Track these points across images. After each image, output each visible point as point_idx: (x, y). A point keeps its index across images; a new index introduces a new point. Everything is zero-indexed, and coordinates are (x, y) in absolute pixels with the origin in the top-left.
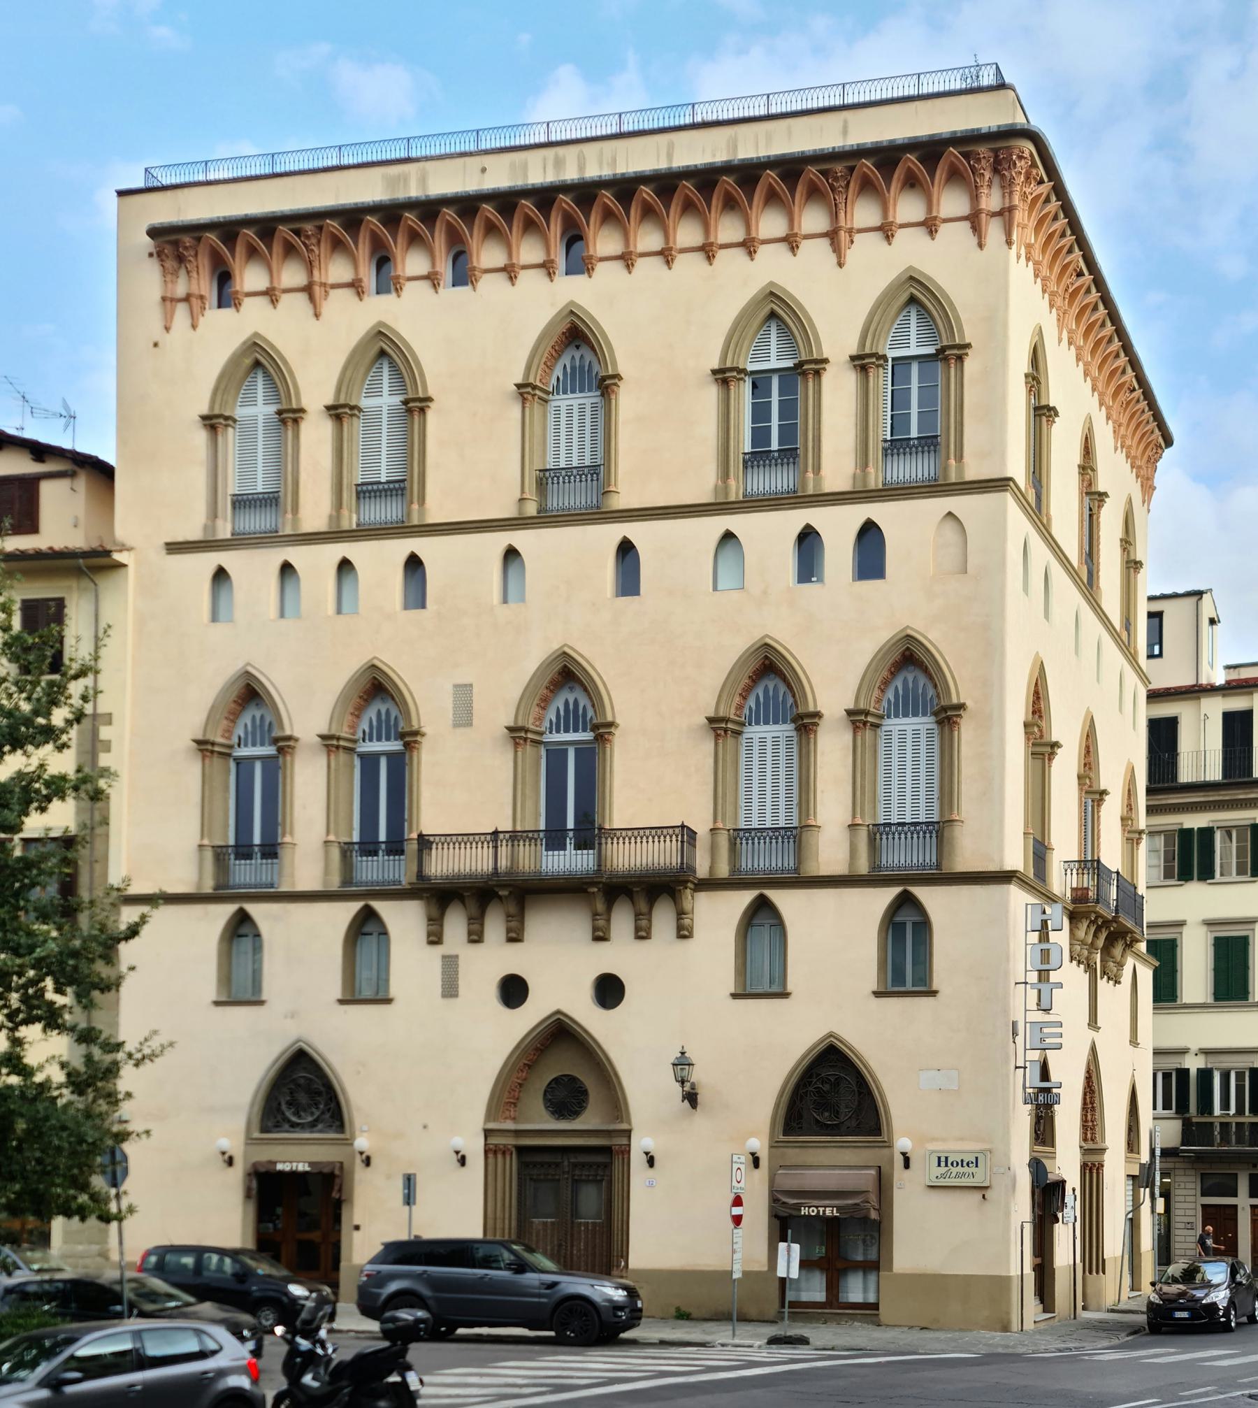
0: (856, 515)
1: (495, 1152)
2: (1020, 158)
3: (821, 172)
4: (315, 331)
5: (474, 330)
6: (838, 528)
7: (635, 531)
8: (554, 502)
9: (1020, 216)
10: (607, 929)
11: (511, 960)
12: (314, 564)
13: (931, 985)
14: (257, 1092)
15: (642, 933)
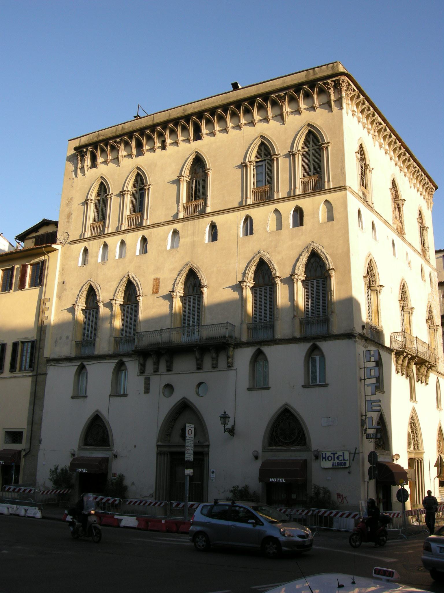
2: (343, 82)
3: (323, 84)
4: (118, 171)
5: (166, 163)
6: (287, 209)
7: (218, 219)
9: (344, 101)
11: (167, 378)
12: (114, 242)
13: (325, 382)
14: (83, 429)
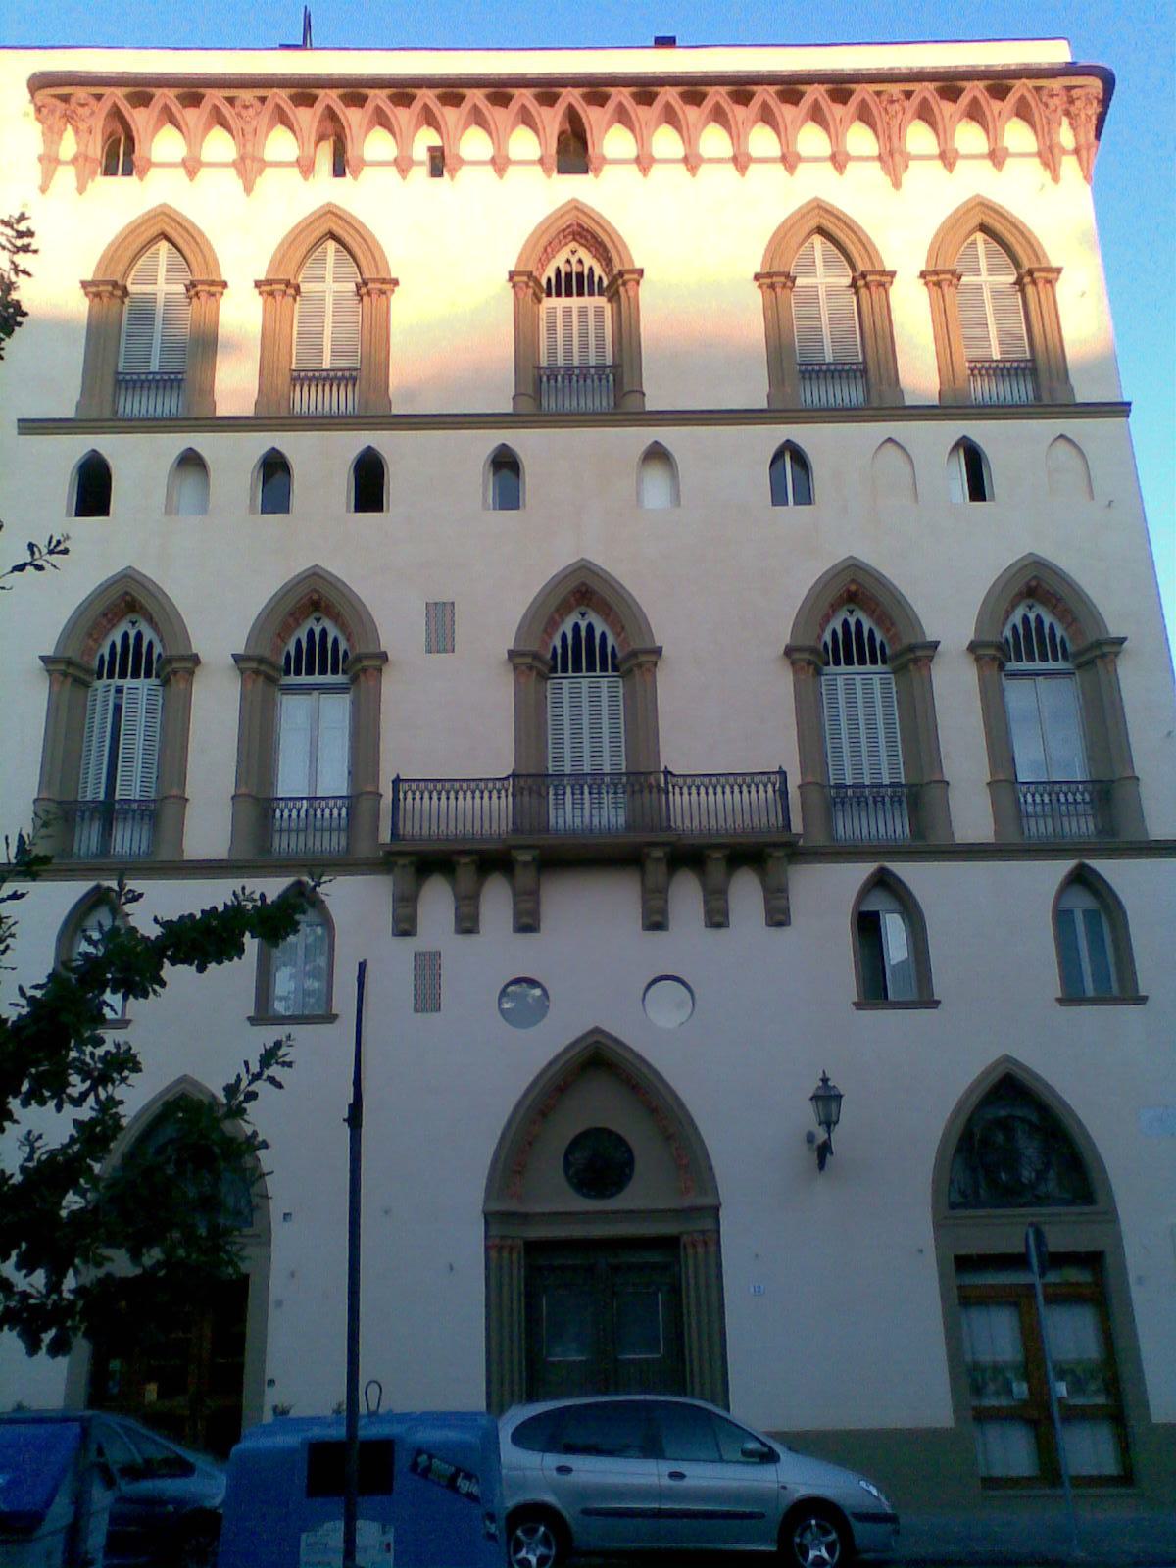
0: (260, 443)
1: (500, 1248)
8: (550, 403)
10: (664, 912)
15: (717, 918)
